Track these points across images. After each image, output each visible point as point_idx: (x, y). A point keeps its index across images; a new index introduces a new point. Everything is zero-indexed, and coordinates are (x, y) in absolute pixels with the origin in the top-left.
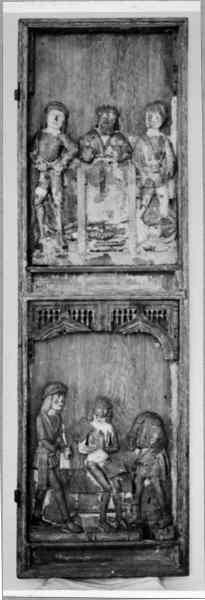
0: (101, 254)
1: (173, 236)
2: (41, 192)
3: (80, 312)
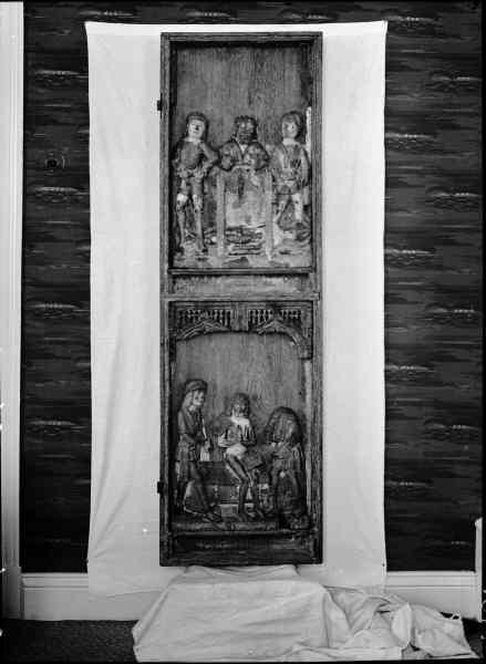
0: (239, 257)
1: (307, 241)
2: (182, 198)
3: (219, 313)
